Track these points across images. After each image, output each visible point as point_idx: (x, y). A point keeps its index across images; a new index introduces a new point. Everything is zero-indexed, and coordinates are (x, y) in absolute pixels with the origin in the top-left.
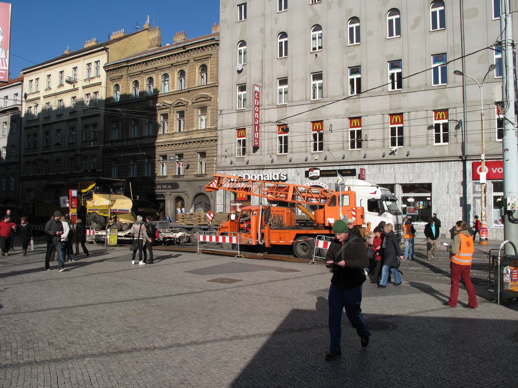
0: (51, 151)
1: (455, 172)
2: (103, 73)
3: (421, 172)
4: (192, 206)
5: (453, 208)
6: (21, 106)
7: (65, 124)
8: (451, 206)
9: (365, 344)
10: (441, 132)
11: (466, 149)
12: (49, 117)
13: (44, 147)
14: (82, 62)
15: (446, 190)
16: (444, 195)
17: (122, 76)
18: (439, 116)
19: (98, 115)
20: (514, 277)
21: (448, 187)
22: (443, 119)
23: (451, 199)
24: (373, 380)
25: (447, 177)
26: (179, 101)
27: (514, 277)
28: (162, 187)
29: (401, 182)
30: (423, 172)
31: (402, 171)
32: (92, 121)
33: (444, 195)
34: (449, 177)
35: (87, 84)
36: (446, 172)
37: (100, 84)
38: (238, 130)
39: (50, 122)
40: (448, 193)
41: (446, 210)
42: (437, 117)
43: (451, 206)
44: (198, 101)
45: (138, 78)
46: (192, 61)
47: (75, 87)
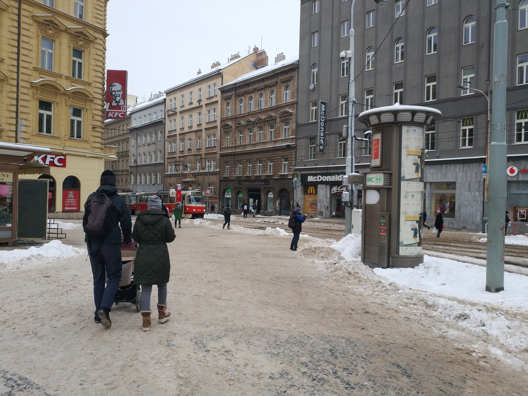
0: (185, 155)
1: (476, 172)
2: (219, 93)
3: (447, 172)
4: (278, 198)
5: (473, 203)
6: (164, 119)
7: (194, 134)
8: (472, 202)
9: (189, 218)
10: (467, 138)
11: (398, 172)
12: (183, 128)
13: (180, 152)
14: (204, 84)
15: (468, 188)
16: (466, 192)
17: (232, 95)
18: (466, 122)
19: (216, 127)
20: (75, 203)
21: (469, 185)
22: (469, 125)
23: (472, 196)
24: (394, 334)
25: (469, 176)
26: (270, 116)
27: (75, 203)
28: (258, 183)
29: (431, 180)
30: (450, 172)
31: (432, 171)
32: (212, 131)
33: (466, 192)
34: (471, 177)
35: (209, 102)
36: (469, 173)
37: (217, 102)
38: (311, 139)
39: (184, 132)
40: (469, 190)
41: (468, 205)
42: (465, 124)
43: (472, 202)
44: (283, 115)
45: (243, 97)
46: (279, 82)
47: (201, 105)
